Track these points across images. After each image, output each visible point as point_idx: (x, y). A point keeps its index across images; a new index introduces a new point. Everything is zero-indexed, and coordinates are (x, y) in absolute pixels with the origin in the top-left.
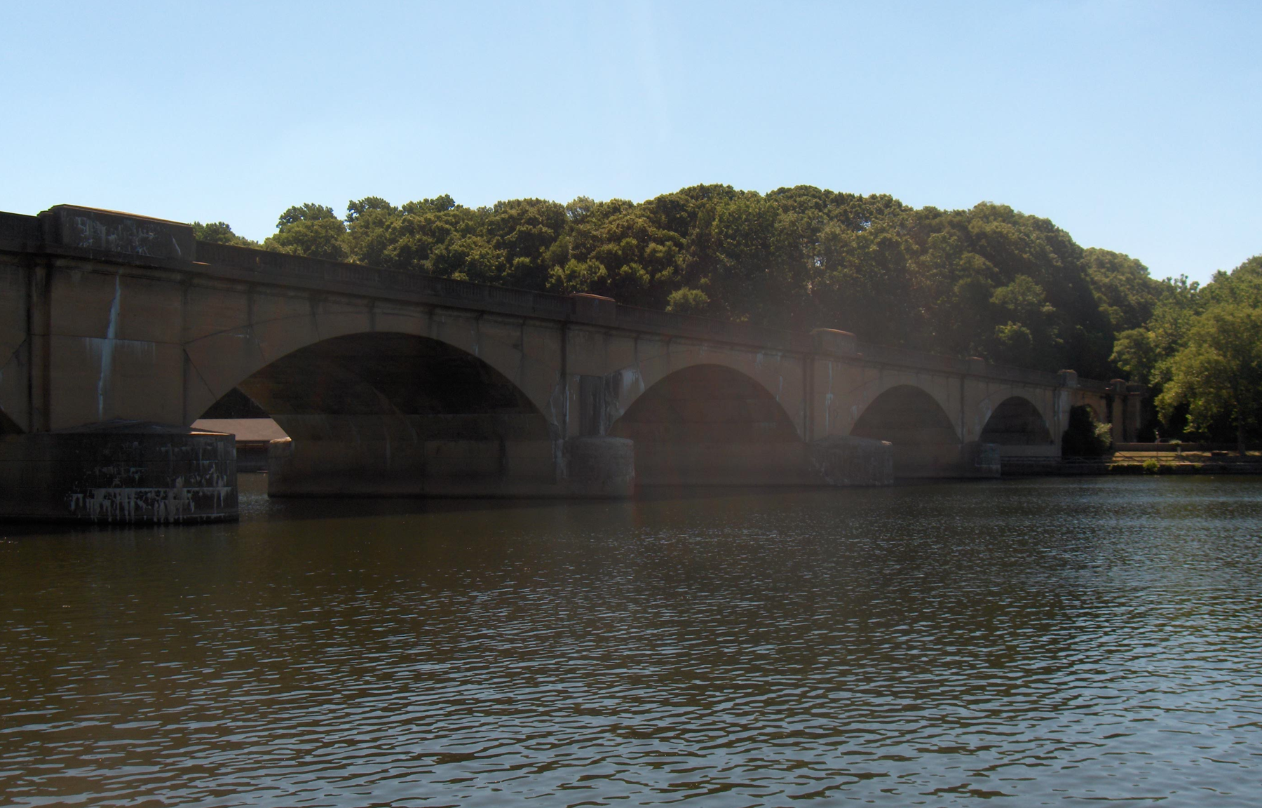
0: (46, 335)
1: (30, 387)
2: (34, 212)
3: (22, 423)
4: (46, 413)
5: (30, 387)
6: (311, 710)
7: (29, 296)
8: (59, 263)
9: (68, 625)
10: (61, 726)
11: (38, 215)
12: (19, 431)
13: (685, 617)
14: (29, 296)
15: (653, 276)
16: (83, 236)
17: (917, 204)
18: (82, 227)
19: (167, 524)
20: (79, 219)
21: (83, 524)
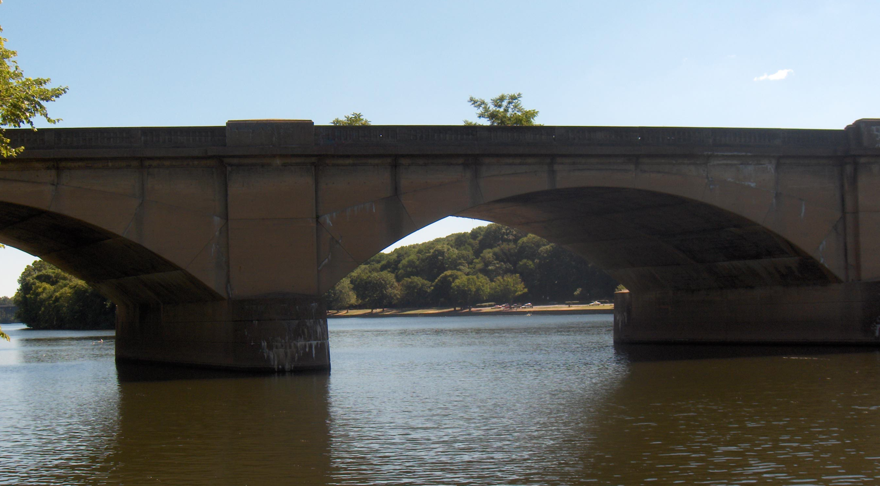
0: (856, 212)
1: (846, 250)
2: (842, 127)
3: (840, 273)
4: (858, 267)
5: (846, 250)
6: (381, 451)
7: (842, 186)
8: (863, 160)
9: (839, 406)
10: (760, 466)
11: (845, 128)
12: (837, 280)
13: (786, 421)
14: (842, 186)
15: (481, 257)
16: (878, 139)
17: (445, 237)
18: (877, 133)
19: (282, 372)
20: (874, 128)
21: (266, 371)
